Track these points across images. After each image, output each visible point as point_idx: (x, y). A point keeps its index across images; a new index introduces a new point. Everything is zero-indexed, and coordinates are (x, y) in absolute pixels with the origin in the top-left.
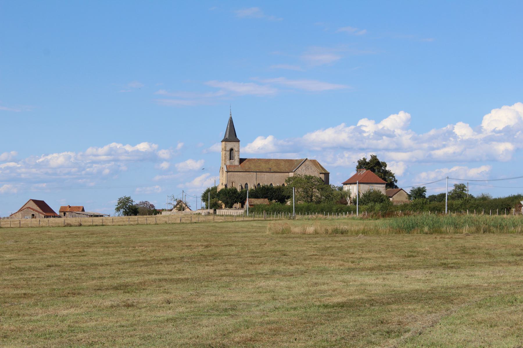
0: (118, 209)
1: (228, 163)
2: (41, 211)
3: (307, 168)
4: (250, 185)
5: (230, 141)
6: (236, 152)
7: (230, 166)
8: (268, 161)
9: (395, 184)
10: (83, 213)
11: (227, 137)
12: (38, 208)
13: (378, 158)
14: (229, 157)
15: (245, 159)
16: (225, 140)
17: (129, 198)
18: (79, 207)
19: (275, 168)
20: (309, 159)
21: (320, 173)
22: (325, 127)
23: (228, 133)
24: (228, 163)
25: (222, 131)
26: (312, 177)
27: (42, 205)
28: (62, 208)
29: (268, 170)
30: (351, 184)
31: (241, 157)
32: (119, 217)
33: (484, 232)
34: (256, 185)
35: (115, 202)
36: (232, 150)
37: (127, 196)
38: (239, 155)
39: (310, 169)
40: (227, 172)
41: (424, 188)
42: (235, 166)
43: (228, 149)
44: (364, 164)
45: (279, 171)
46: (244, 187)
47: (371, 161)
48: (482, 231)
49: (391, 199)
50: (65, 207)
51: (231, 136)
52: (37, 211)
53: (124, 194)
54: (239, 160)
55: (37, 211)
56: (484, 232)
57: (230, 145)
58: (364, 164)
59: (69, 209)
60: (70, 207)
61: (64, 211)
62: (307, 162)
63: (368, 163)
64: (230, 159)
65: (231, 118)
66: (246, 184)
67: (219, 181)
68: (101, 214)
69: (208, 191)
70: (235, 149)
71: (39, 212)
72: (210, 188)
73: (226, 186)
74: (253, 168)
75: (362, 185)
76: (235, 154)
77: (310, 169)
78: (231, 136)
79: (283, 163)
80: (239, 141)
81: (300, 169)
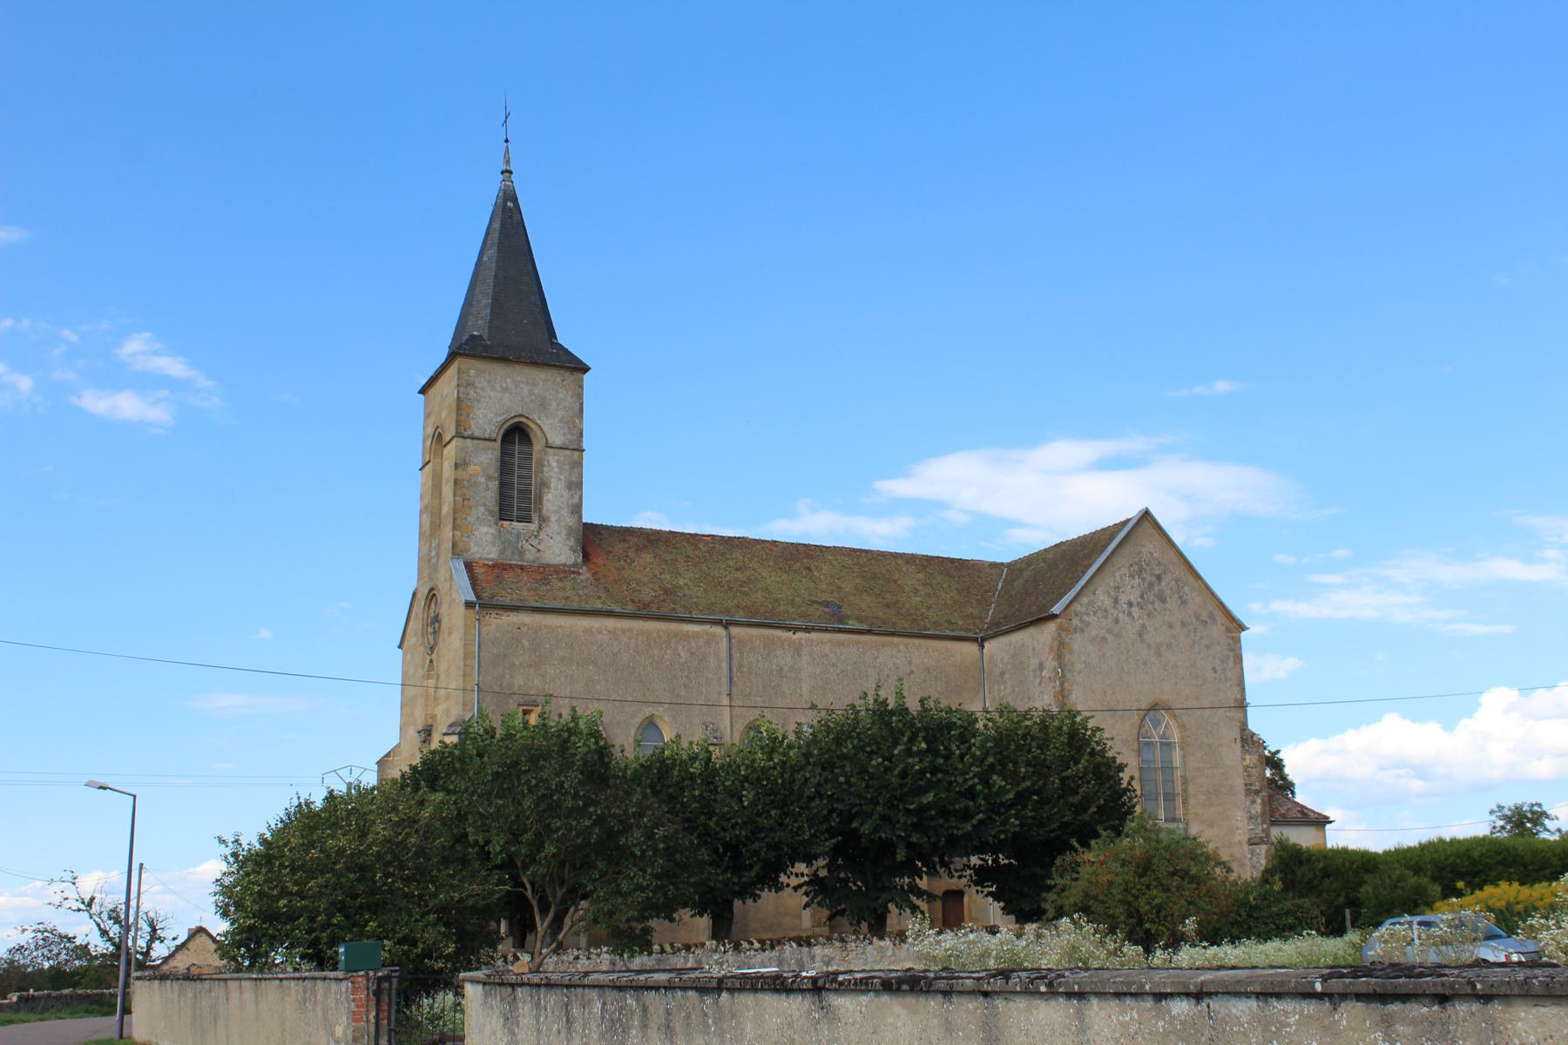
1: (485, 542)
5: (504, 359)
7: (499, 568)
11: (479, 328)
14: (488, 493)
22: (1013, 426)
23: (485, 302)
24: (485, 542)
36: (516, 434)
39: (1172, 603)
42: (544, 572)
43: (488, 418)
51: (509, 318)
57: (503, 393)
70: (549, 428)
72: (318, 803)
77: (1172, 603)
78: (509, 318)
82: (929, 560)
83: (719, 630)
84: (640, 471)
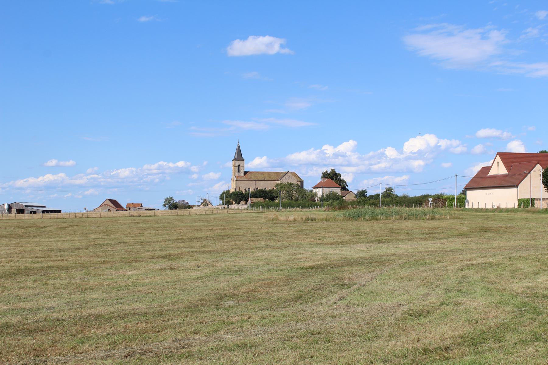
0: (164, 205)
1: (237, 174)
8: (263, 173)
14: (237, 170)
18: (139, 204)
24: (237, 174)
25: (233, 154)
28: (127, 204)
29: (263, 179)
33: (405, 219)
35: (163, 201)
36: (239, 166)
37: (171, 197)
40: (236, 180)
42: (241, 177)
43: (237, 165)
47: (331, 173)
51: (239, 157)
53: (168, 196)
56: (405, 219)
57: (238, 163)
62: (289, 174)
66: (249, 188)
69: (224, 193)
70: (242, 165)
73: (235, 190)
74: (253, 178)
75: (325, 189)
76: (242, 168)
78: (239, 157)
80: (244, 160)
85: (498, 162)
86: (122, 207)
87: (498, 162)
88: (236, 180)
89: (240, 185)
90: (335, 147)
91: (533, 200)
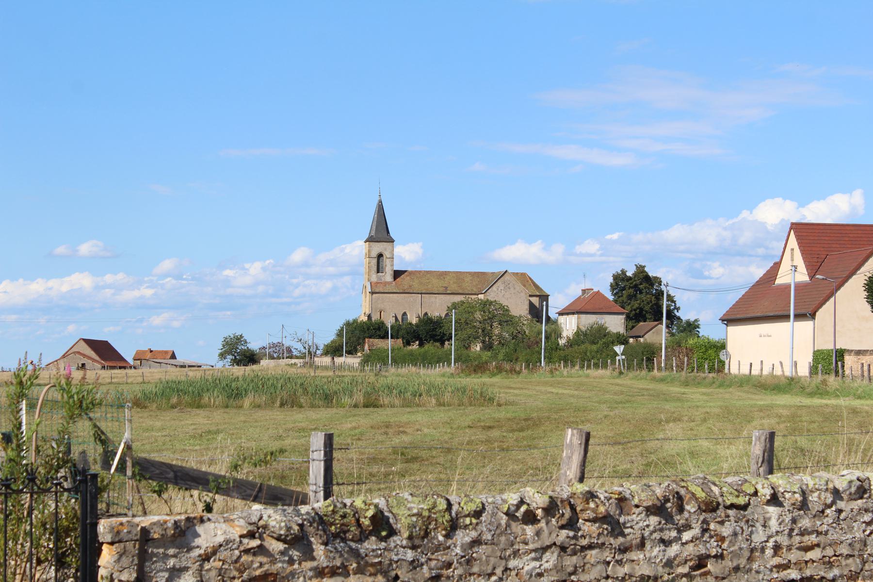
0: (222, 356)
1: (374, 278)
2: (97, 358)
3: (507, 287)
4: (411, 316)
6: (388, 260)
8: (443, 275)
9: (678, 314)
10: (172, 361)
11: (373, 234)
12: (93, 352)
13: (646, 269)
14: (375, 268)
15: (404, 272)
16: (370, 240)
17: (241, 336)
18: (166, 352)
19: (454, 287)
20: (510, 271)
21: (530, 296)
23: (374, 227)
24: (374, 278)
25: (366, 224)
26: (491, 302)
27: (104, 351)
28: (138, 353)
29: (441, 290)
30: (568, 314)
31: (396, 268)
32: (225, 367)
33: (282, 405)
34: (422, 316)
35: (217, 346)
36: (380, 256)
37: (238, 334)
38: (392, 265)
39: (512, 289)
40: (372, 293)
41: (696, 321)
42: (386, 284)
43: (374, 254)
44: (623, 280)
45: (460, 291)
46: (400, 319)
47: (635, 275)
48: (278, 403)
49: (642, 340)
50: (144, 352)
51: (381, 232)
52: (90, 358)
53: (231, 332)
54: (392, 273)
55: (90, 358)
56: (282, 405)
57: (378, 248)
58: (623, 280)
59: (149, 355)
60: (151, 351)
61: (140, 358)
62: (506, 277)
63: (630, 278)
64: (378, 272)
65: (380, 202)
66: (405, 314)
67: (360, 310)
68: (199, 363)
69: (348, 324)
70: (387, 254)
71: (94, 360)
73: (369, 317)
74: (416, 286)
75: (583, 316)
76: (386, 262)
77: (512, 289)
78: (381, 232)
79: (468, 279)
80: (393, 241)
81: (494, 288)
82: (475, 273)
83: (254, 493)
84: (405, 254)
85: (792, 250)
86: (122, 359)
87: (792, 250)
88: (372, 293)
89: (381, 306)
90: (802, 204)
91: (840, 354)
